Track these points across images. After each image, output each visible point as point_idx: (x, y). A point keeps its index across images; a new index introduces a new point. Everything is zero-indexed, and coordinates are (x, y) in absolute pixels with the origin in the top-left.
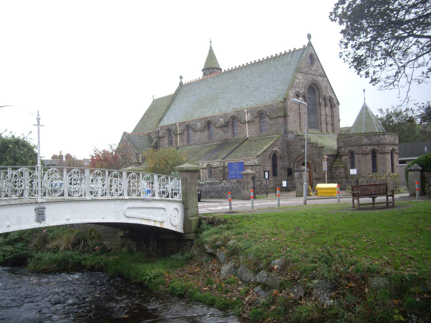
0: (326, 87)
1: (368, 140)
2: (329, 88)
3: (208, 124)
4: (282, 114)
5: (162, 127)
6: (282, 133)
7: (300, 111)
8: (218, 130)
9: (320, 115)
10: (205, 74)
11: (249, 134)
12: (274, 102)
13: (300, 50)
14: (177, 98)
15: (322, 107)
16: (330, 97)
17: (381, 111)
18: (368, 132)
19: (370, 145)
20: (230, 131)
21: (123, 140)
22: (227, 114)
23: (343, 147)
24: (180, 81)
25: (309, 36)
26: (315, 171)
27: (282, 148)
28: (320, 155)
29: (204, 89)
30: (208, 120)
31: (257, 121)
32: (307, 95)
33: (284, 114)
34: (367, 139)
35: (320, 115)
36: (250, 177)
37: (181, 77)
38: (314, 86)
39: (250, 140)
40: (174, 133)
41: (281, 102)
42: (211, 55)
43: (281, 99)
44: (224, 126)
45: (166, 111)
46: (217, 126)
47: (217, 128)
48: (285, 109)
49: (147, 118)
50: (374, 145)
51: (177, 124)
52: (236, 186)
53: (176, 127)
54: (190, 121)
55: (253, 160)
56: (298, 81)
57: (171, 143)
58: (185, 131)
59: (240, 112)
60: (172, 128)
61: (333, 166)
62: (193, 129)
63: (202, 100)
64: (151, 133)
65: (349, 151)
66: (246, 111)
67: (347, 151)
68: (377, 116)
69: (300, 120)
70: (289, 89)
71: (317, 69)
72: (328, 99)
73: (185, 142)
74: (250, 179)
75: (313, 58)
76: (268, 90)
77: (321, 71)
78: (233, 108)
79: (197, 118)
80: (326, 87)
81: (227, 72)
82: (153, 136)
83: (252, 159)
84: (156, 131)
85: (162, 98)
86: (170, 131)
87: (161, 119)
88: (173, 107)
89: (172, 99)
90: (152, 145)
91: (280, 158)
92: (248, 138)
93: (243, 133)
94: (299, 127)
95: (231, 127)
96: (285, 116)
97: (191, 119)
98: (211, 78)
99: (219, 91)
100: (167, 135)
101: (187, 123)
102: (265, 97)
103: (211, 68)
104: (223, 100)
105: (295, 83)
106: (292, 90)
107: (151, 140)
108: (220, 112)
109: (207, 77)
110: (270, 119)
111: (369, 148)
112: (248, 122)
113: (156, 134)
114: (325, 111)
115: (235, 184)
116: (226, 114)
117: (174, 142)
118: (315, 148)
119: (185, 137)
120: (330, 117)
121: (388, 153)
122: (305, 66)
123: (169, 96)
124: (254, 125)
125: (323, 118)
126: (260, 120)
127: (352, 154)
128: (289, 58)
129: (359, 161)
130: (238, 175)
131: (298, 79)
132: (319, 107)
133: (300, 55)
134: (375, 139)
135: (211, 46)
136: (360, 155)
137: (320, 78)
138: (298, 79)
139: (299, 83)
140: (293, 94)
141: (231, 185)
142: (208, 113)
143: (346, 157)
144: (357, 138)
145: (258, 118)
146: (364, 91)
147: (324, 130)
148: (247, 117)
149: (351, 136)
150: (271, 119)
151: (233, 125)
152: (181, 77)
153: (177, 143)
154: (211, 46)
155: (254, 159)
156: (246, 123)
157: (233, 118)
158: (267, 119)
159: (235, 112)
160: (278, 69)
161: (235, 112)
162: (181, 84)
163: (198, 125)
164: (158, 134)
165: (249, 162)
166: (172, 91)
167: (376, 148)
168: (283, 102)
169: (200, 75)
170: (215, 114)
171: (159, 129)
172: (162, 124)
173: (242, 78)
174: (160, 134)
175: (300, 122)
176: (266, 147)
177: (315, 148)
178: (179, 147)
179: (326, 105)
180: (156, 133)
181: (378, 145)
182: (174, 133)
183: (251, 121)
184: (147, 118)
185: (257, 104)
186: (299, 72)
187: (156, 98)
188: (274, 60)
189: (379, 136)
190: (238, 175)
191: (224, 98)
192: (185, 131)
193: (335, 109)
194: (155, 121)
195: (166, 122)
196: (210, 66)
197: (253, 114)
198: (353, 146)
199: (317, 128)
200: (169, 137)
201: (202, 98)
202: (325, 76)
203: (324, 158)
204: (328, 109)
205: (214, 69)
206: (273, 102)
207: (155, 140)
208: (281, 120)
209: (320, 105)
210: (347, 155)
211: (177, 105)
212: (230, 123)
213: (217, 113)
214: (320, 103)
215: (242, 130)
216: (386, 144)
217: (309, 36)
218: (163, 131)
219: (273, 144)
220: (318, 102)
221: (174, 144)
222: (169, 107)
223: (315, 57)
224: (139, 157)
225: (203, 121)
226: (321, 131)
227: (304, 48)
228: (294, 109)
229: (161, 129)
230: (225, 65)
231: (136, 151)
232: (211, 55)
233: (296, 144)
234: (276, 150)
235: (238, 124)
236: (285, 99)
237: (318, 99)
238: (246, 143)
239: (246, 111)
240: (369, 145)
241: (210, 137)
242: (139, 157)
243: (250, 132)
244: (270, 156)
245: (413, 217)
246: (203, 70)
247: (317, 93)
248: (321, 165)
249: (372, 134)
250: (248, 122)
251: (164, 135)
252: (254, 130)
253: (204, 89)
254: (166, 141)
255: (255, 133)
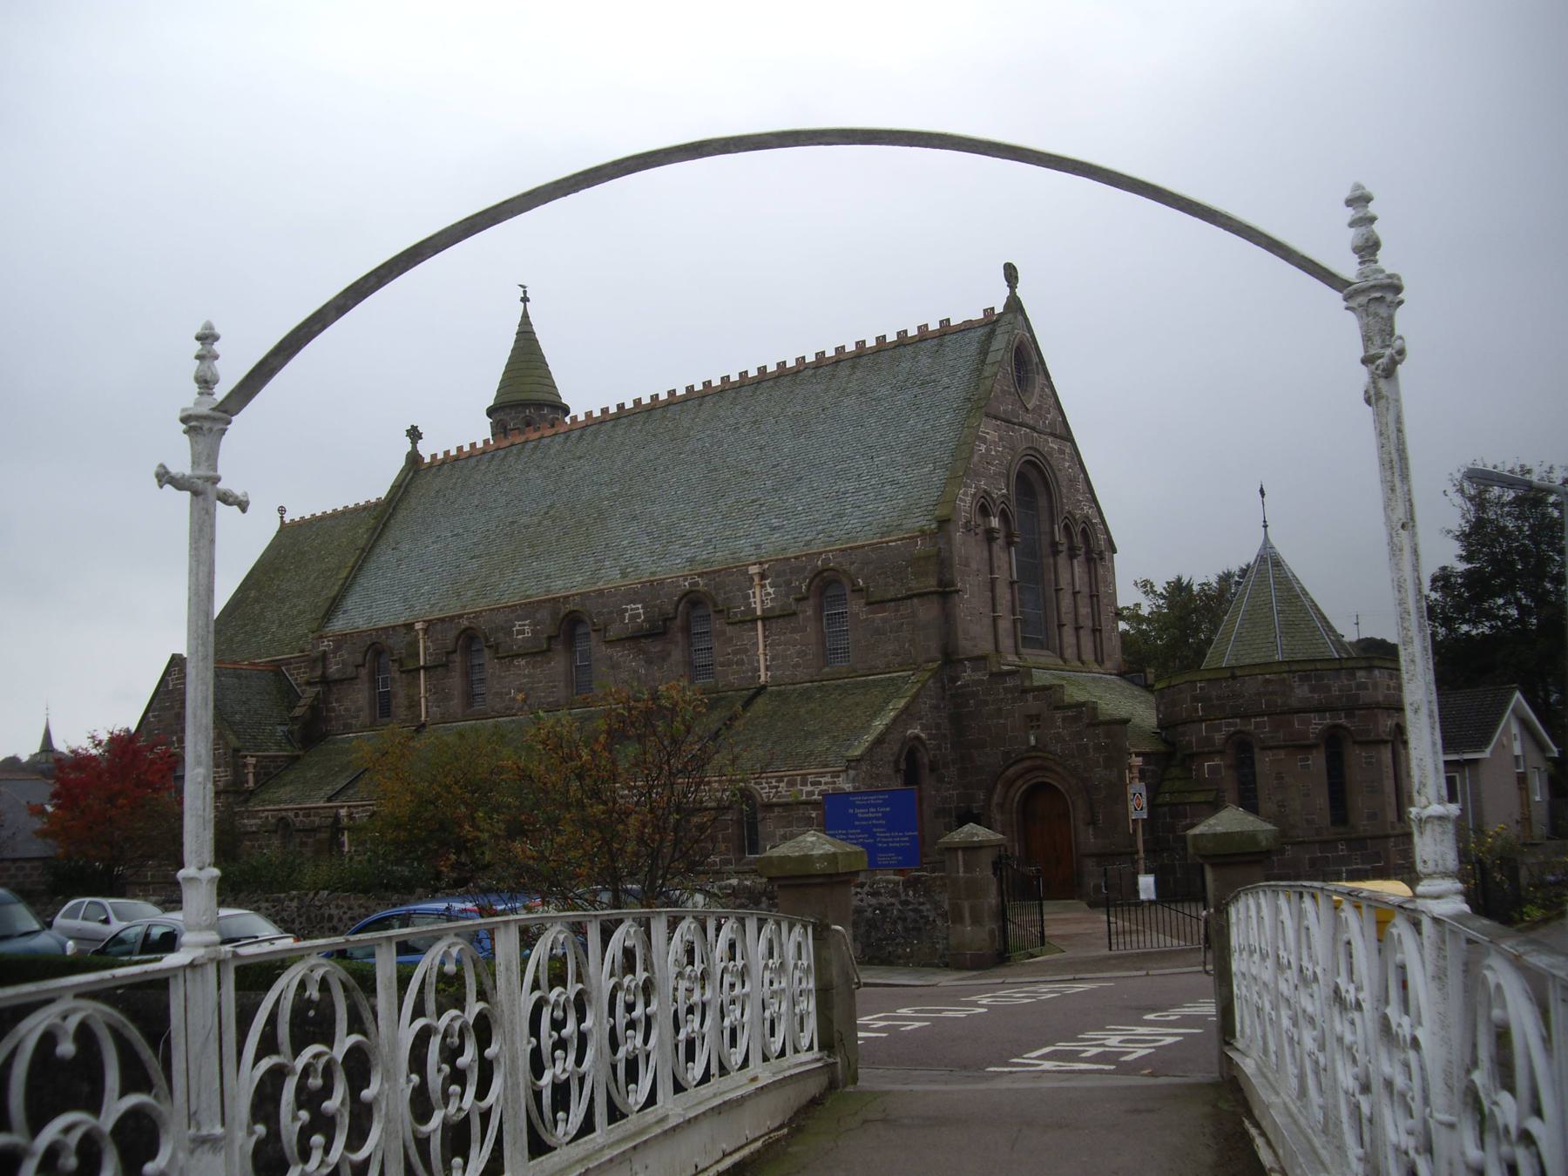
0: (1072, 480)
1: (1313, 689)
2: (1081, 486)
3: (569, 625)
4: (931, 583)
5: (342, 640)
6: (935, 665)
7: (992, 572)
8: (617, 653)
9: (1057, 591)
10: (499, 429)
11: (767, 668)
12: (889, 533)
13: (968, 326)
14: (399, 517)
15: (1062, 559)
16: (1087, 520)
17: (1147, 587)
18: (1299, 657)
19: (1320, 710)
20: (677, 655)
21: (169, 692)
22: (661, 582)
23: (1201, 720)
24: (409, 448)
25: (1011, 273)
26: (1092, 822)
27: (938, 726)
28: (1115, 758)
29: (528, 480)
30: (570, 607)
31: (810, 612)
32: (1013, 508)
33: (940, 583)
34: (1306, 688)
35: (1057, 591)
36: (987, 858)
37: (414, 434)
38: (1033, 475)
39: (780, 693)
40: (400, 662)
41: (923, 532)
42: (526, 352)
43: (920, 521)
44: (646, 636)
45: (357, 569)
46: (611, 635)
47: (610, 643)
48: (942, 563)
49: (257, 600)
50: (1332, 709)
51: (418, 626)
52: (905, 903)
53: (408, 638)
54: (478, 614)
55: (827, 779)
56: (983, 447)
57: (383, 707)
58: (457, 658)
59: (735, 574)
60: (390, 642)
61: (1160, 800)
62: (495, 648)
63: (527, 527)
64: (288, 662)
65: (1230, 737)
66: (753, 570)
67: (1219, 737)
68: (1138, 605)
69: (994, 611)
70: (955, 479)
71: (1040, 407)
72: (1079, 529)
73: (456, 704)
74: (985, 873)
75: (1026, 361)
76: (851, 486)
77: (1052, 414)
78: (691, 560)
79: (516, 600)
80: (1072, 480)
81: (631, 413)
82: (298, 677)
83: (823, 775)
84: (314, 654)
85: (324, 517)
86: (378, 650)
87: (334, 606)
88: (385, 555)
89: (374, 525)
90: (298, 712)
91: (932, 770)
92: (764, 687)
93: (740, 663)
94: (991, 638)
95: (679, 637)
96: (946, 592)
97: (483, 604)
98: (560, 439)
99: (606, 492)
100: (364, 672)
101: (465, 623)
102: (841, 516)
103: (526, 397)
104: (633, 527)
105: (976, 458)
106: (966, 486)
107: (289, 695)
108: (624, 575)
109: (536, 435)
110: (868, 604)
111: (1316, 725)
112: (764, 619)
113: (312, 670)
114: (1071, 574)
115: (895, 894)
116: (654, 586)
117: (400, 700)
118: (1090, 725)
119: (455, 682)
120: (1087, 601)
121: (1386, 742)
122: (1003, 391)
123: (358, 510)
124: (794, 631)
125: (1066, 601)
126: (819, 609)
127: (1243, 750)
128: (925, 361)
129: (1279, 777)
130: (883, 850)
131: (984, 441)
132: (1051, 561)
133: (973, 349)
134: (1336, 686)
135: (525, 316)
136: (1282, 754)
137: (1054, 445)
138: (984, 441)
139: (987, 460)
140: (968, 499)
141: (873, 901)
142: (566, 579)
143: (1217, 761)
144: (1268, 681)
145: (811, 601)
146: (1262, 492)
147: (1070, 652)
148: (760, 598)
149: (1238, 673)
150: (875, 604)
151: (687, 630)
152: (414, 434)
153: (413, 705)
154: (525, 316)
155: (836, 775)
156: (754, 621)
157: (693, 600)
158: (856, 606)
159: (699, 575)
160: (878, 400)
161: (699, 575)
162: (414, 459)
163: (519, 632)
164: (325, 667)
165: (809, 788)
166: (376, 487)
167: (1343, 721)
168: (933, 534)
169: (480, 431)
170: (600, 585)
171: (326, 645)
172: (339, 624)
173: (712, 436)
174: (333, 669)
175: (995, 619)
176: (879, 724)
177: (1090, 725)
178: (424, 725)
179: (1072, 556)
180: (315, 660)
181: (1350, 712)
182: (400, 662)
183: (777, 613)
184: (257, 600)
185: (807, 544)
186: (987, 415)
187: (292, 515)
188: (853, 367)
189: (1352, 672)
190: (883, 850)
191: (635, 518)
192: (457, 658)
193: (1101, 571)
194: (301, 612)
195: (357, 616)
196: (523, 396)
197: (788, 583)
198: (1246, 717)
199: (1043, 645)
200: (373, 681)
201: (525, 520)
202: (1067, 437)
203: (1130, 768)
204: (1079, 567)
205: (539, 405)
206: (883, 535)
207: (311, 692)
208: (927, 612)
209: (1056, 553)
210: (1221, 753)
211: (405, 547)
212: (678, 622)
213: (611, 577)
214: (1054, 544)
215: (735, 653)
216: (1378, 706)
217: (1011, 273)
218: (344, 654)
219: (906, 708)
220: (1045, 540)
221: (402, 713)
222: (366, 553)
223: (1036, 359)
224: (245, 765)
225: (544, 614)
226: (1062, 656)
227: (991, 322)
228: (974, 566)
229: (338, 648)
230: (585, 388)
231: (231, 737)
232: (526, 352)
233: (1000, 709)
234: (917, 738)
235: (718, 624)
236: (943, 522)
237: (1045, 527)
238: (760, 704)
239: (753, 570)
240: (1317, 710)
241: (580, 681)
242: (245, 765)
243: (773, 659)
244: (897, 762)
245: (1343, 988)
246: (491, 412)
247: (1042, 502)
248: (1118, 794)
249: (1326, 665)
250: (764, 619)
251: (350, 671)
252: (792, 650)
253: (528, 480)
254: (359, 698)
255: (797, 666)
